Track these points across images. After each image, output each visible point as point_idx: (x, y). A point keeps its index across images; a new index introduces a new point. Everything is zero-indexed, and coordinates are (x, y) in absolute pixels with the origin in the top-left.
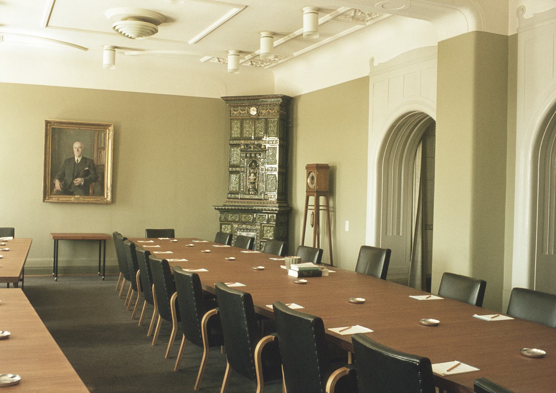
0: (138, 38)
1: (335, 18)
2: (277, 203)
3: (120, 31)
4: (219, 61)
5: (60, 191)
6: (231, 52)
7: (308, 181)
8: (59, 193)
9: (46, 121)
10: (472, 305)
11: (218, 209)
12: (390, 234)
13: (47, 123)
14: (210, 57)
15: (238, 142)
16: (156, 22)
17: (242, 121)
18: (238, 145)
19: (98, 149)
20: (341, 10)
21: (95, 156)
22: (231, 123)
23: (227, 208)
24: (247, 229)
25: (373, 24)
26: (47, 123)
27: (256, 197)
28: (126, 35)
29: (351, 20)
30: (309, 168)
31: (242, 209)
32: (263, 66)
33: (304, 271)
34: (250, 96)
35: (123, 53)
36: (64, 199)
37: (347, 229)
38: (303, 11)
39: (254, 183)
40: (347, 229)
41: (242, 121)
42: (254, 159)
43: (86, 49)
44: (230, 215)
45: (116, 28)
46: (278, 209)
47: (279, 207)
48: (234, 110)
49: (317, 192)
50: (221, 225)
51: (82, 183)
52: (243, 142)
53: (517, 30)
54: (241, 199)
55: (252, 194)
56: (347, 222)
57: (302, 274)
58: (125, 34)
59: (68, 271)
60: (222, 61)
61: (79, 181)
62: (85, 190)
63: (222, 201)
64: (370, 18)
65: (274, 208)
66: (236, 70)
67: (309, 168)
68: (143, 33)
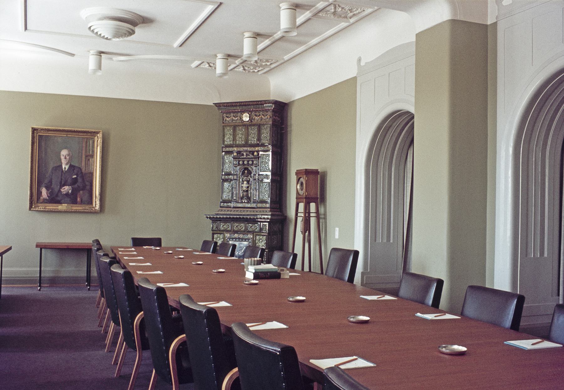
0: (114, 39)
1: (316, 15)
2: (271, 211)
3: (95, 31)
4: (210, 66)
5: (46, 199)
6: (220, 56)
7: (298, 187)
8: (45, 201)
9: (32, 128)
10: (428, 305)
11: (210, 218)
12: (379, 240)
13: (34, 130)
14: (200, 62)
15: (231, 149)
16: (134, 24)
17: (235, 128)
18: (231, 152)
19: (86, 156)
20: (321, 5)
21: (83, 164)
22: (224, 129)
23: (221, 216)
24: (239, 238)
25: (357, 21)
26: (34, 130)
27: (249, 205)
28: (102, 35)
29: (332, 16)
30: (298, 173)
31: (234, 218)
32: (256, 71)
33: (261, 272)
34: (242, 102)
35: (111, 59)
36: (51, 208)
37: (337, 237)
38: (280, 8)
39: (247, 191)
40: (337, 237)
41: (235, 128)
42: (246, 166)
43: (73, 55)
44: (222, 224)
45: (92, 28)
46: (270, 217)
47: (271, 215)
48: (227, 117)
49: (306, 198)
50: (213, 234)
51: (70, 191)
52: (235, 149)
53: (497, 18)
54: (234, 207)
55: (245, 202)
56: (337, 229)
57: (257, 275)
58: (100, 35)
59: (54, 282)
60: (212, 65)
61: (66, 189)
62: (72, 198)
63: (214, 211)
64: (352, 14)
65: (266, 217)
66: (224, 74)
67: (298, 173)
68: (118, 34)
